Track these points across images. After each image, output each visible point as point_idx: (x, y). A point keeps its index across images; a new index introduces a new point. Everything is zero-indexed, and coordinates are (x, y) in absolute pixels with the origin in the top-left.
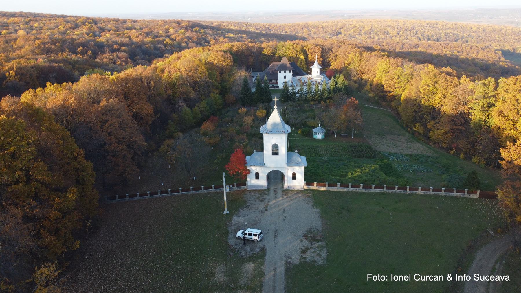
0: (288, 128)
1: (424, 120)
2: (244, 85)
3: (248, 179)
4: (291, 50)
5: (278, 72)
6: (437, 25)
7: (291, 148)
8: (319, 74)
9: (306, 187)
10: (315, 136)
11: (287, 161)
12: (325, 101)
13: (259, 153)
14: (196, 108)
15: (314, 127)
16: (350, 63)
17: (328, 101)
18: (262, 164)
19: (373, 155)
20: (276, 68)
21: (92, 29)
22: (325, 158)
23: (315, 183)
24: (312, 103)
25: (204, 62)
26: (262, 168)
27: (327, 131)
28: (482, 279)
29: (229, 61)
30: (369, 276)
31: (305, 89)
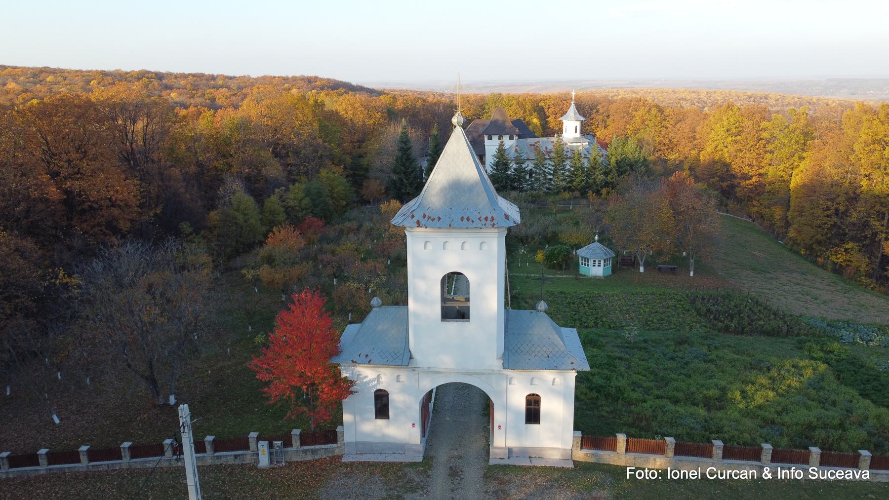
0: (511, 211)
1: (868, 233)
2: (402, 149)
3: (347, 417)
4: (514, 107)
5: (486, 138)
6: (766, 98)
7: (516, 299)
8: (578, 135)
9: (582, 455)
10: (583, 269)
11: (506, 348)
12: (598, 193)
13: (393, 309)
14: (274, 198)
15: (578, 246)
16: (639, 130)
17: (604, 191)
18: (402, 358)
19: (785, 328)
20: (481, 130)
21: (150, 86)
22: (633, 333)
23: (621, 438)
24: (567, 195)
25: (311, 102)
26: (404, 375)
27: (618, 254)
28: (823, 476)
29: (378, 115)
30: (630, 470)
31: (549, 165)
